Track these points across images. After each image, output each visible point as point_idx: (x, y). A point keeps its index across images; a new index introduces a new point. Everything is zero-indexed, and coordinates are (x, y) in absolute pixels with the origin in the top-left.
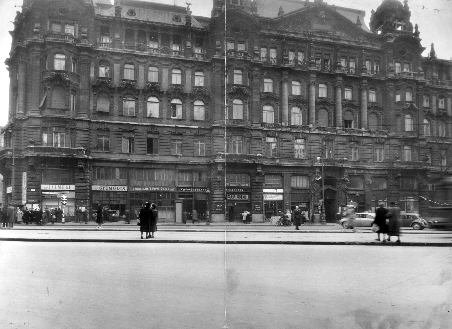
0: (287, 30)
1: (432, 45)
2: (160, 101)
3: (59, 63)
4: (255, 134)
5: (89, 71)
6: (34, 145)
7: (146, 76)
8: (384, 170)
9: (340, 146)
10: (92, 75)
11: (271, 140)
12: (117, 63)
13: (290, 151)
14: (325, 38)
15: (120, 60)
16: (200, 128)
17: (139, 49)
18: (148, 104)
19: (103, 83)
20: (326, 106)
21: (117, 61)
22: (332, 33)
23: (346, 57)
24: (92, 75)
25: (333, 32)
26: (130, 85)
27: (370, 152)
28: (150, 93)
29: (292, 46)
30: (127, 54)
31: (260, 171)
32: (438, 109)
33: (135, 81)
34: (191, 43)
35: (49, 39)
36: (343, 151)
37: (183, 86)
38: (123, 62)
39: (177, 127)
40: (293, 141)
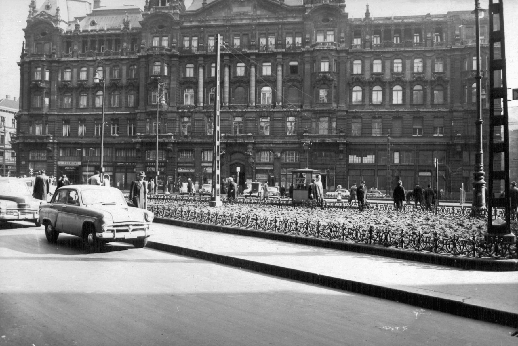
0: (208, 19)
1: (367, 6)
2: (88, 94)
3: (324, 67)
4: (169, 115)
5: (58, 77)
6: (308, 133)
7: (433, 69)
8: (294, 143)
9: (249, 121)
10: (60, 79)
11: (186, 119)
12: (408, 59)
13: (201, 129)
14: (244, 19)
15: (76, 66)
16: (130, 114)
17: (406, 46)
18: (373, 93)
19: (66, 85)
20: (242, 84)
21: (75, 67)
22: (252, 13)
23: (292, 33)
24: (60, 79)
25: (254, 11)
26: (82, 84)
27: (280, 126)
28: (375, 84)
29: (211, 32)
30: (81, 61)
31: (342, 149)
32: (372, 74)
33: (119, 80)
34: (127, 44)
35: (317, 48)
36: (251, 126)
37: (119, 80)
38: (111, 66)
39: (114, 114)
40: (230, 119)
